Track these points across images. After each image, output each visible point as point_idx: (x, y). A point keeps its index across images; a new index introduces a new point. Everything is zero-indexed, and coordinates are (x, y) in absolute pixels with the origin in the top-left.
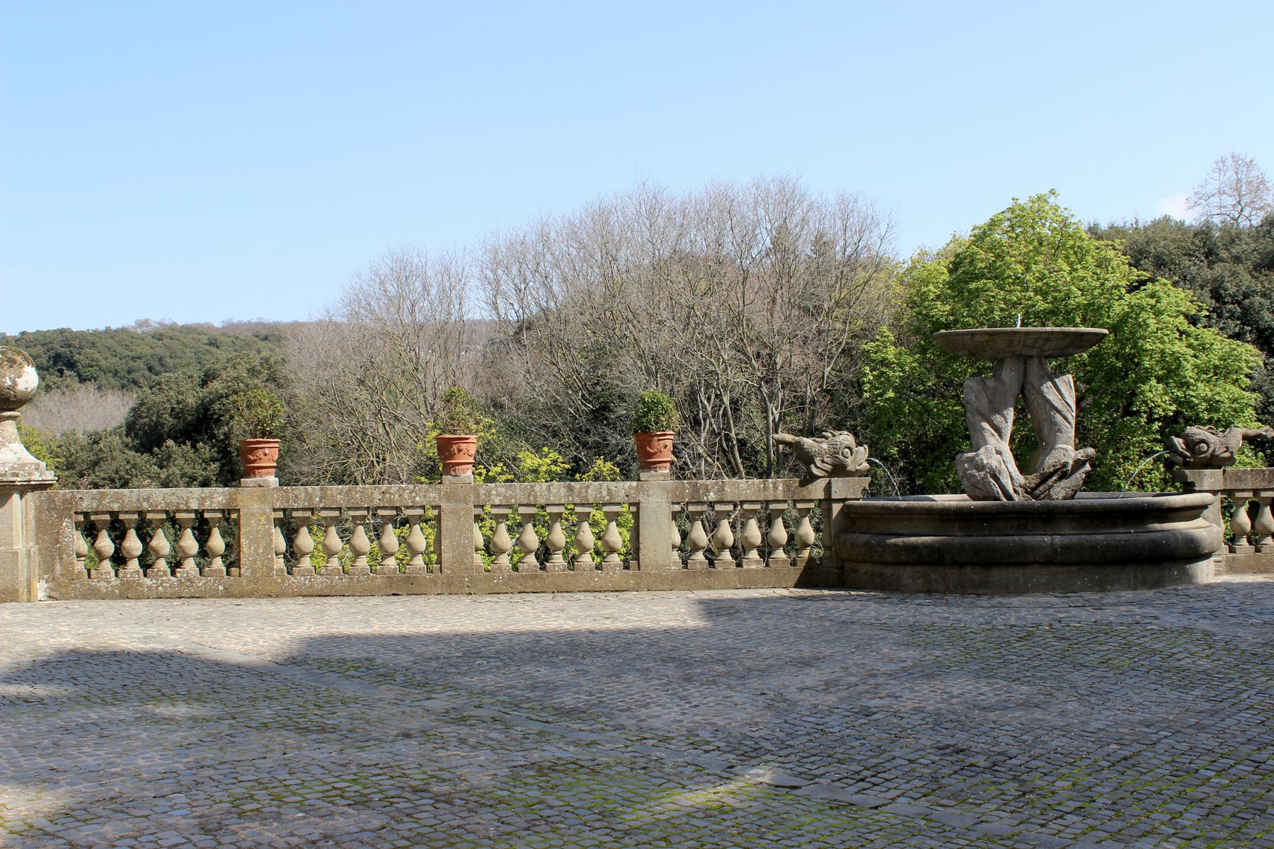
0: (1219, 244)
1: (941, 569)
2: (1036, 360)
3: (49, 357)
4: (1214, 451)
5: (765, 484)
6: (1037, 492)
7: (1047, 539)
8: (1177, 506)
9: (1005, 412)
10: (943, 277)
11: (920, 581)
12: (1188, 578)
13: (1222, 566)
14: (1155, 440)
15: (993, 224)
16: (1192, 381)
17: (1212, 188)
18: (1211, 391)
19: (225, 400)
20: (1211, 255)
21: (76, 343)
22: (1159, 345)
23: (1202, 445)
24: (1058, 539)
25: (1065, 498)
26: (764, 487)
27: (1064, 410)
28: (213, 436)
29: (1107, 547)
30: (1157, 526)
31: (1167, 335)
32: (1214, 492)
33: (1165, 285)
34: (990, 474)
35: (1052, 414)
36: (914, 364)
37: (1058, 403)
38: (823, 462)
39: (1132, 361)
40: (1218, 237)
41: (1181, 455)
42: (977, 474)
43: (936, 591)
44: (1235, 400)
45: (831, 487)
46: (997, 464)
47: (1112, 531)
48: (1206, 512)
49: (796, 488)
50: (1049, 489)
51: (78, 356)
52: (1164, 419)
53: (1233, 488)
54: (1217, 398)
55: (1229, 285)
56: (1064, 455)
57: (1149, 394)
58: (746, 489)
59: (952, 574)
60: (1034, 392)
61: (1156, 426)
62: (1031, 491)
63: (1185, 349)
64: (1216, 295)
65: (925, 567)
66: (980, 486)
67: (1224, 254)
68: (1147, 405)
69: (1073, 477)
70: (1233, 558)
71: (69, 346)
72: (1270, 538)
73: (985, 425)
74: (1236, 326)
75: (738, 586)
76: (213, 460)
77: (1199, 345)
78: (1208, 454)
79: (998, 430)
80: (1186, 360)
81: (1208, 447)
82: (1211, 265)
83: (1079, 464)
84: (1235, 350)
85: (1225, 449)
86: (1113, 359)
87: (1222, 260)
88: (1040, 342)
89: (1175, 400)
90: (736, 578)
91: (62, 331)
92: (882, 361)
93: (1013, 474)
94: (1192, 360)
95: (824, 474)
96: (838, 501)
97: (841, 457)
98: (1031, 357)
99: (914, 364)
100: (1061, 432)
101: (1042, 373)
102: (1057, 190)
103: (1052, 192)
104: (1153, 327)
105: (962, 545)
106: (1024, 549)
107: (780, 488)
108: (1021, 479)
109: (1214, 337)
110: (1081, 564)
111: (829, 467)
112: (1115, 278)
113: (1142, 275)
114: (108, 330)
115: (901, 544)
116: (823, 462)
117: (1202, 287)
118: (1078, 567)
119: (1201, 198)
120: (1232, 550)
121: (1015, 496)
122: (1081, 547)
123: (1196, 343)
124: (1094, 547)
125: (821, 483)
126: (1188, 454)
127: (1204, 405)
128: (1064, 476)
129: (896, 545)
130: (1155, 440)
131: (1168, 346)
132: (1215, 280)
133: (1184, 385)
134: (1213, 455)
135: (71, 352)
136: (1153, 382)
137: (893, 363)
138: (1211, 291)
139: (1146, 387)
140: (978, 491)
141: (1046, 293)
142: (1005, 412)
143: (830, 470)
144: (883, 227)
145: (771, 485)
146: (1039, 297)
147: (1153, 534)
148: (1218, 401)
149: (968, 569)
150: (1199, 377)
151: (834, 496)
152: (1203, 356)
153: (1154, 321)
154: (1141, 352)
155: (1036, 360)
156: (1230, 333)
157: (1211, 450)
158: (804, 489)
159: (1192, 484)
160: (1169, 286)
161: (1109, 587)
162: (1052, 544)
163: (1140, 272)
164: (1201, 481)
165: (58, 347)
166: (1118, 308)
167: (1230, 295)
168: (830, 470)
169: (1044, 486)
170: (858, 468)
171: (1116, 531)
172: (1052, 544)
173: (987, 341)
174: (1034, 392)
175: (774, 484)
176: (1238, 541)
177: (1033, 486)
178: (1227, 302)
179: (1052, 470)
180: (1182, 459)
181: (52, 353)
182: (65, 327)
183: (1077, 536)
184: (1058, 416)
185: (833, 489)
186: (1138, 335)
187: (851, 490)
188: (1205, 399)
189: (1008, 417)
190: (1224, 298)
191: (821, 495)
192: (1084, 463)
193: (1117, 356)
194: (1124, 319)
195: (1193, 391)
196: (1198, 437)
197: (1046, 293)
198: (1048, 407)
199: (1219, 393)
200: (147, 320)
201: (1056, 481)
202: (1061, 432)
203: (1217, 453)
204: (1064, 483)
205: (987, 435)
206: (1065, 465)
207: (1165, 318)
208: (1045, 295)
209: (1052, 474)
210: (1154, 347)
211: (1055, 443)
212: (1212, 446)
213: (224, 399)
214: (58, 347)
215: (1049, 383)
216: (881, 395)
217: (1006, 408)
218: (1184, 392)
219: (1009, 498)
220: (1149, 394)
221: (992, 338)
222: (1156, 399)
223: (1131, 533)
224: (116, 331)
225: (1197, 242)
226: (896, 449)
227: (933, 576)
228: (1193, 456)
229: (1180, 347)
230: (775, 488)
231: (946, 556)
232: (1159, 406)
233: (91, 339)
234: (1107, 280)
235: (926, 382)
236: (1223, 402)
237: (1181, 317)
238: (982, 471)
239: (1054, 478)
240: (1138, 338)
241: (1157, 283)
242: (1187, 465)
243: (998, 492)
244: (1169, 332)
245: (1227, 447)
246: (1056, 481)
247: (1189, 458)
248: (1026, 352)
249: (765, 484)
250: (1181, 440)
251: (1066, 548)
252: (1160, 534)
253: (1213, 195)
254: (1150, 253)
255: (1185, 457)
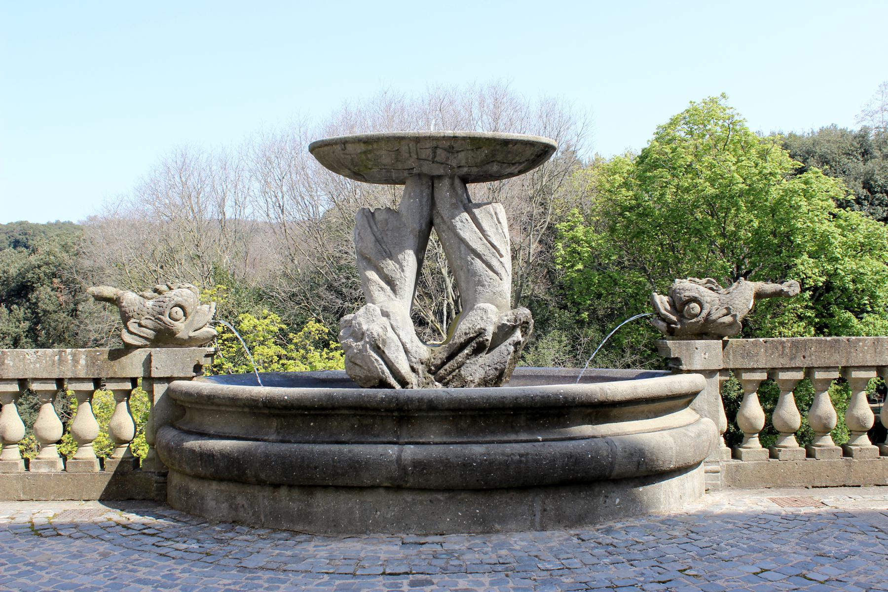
0: (874, 145)
1: (249, 490)
2: (446, 182)
3: (10, 242)
4: (709, 314)
5: (61, 356)
6: (442, 371)
7: (392, 451)
8: (619, 398)
9: (400, 257)
10: (628, 168)
11: (224, 506)
12: (636, 508)
13: (720, 480)
14: (807, 307)
15: (674, 122)
16: (839, 256)
17: (876, 106)
18: (857, 264)
19: (37, 270)
20: (866, 154)
21: (31, 232)
22: (809, 224)
23: (693, 305)
24: (410, 452)
25: (485, 382)
26: (59, 359)
27: (486, 253)
28: (29, 300)
29: (488, 465)
30: (587, 429)
31: (817, 216)
32: (709, 373)
33: (817, 173)
34: (371, 345)
35: (469, 259)
36: (600, 241)
37: (477, 244)
38: (140, 325)
39: (788, 237)
40: (873, 140)
41: (664, 319)
42: (354, 345)
43: (242, 523)
44: (877, 273)
45: (151, 362)
46: (380, 331)
47: (505, 438)
48: (697, 401)
49: (104, 361)
50: (459, 367)
51: (31, 242)
52: (815, 289)
53: (738, 366)
54: (861, 270)
55: (878, 177)
56: (482, 319)
57: (801, 267)
58: (35, 363)
59: (264, 498)
60: (445, 228)
61: (807, 294)
62: (435, 370)
63: (833, 228)
64: (867, 185)
65: (231, 485)
66: (358, 362)
67: (877, 153)
68: (800, 276)
69: (497, 350)
70: (737, 466)
71: (26, 234)
72: (792, 438)
73: (372, 275)
74: (884, 211)
75: (22, 497)
76: (26, 319)
77: (848, 226)
78: (700, 318)
79: (390, 282)
80: (834, 237)
81: (702, 308)
82: (865, 161)
83: (504, 332)
84: (878, 229)
85: (725, 311)
86: (771, 237)
87: (875, 157)
88: (441, 155)
89: (823, 273)
90: (19, 486)
91: (21, 223)
92: (572, 238)
93: (408, 346)
94: (840, 238)
95: (144, 342)
96: (161, 380)
97: (166, 319)
98: (440, 177)
99: (600, 241)
100: (483, 286)
101: (454, 201)
102: (728, 94)
103: (723, 96)
104: (804, 209)
105: (267, 456)
106: (356, 466)
107: (82, 362)
108: (422, 351)
109: (860, 218)
110: (450, 489)
111: (150, 334)
112: (772, 167)
113: (796, 164)
114: (57, 223)
115: (197, 449)
116: (140, 325)
117: (855, 180)
118: (447, 495)
119: (867, 115)
120: (735, 455)
121: (411, 377)
122: (445, 465)
123: (844, 224)
124: (466, 465)
125: (139, 356)
126: (674, 318)
127: (849, 278)
128: (480, 349)
129: (192, 451)
130: (807, 307)
131: (818, 225)
132: (868, 173)
133: (833, 260)
134: (707, 319)
135: (27, 239)
136: (805, 257)
137: (582, 240)
138: (864, 183)
139: (798, 261)
140: (358, 368)
141: (714, 180)
142: (400, 257)
143: (152, 337)
144: (580, 125)
145: (70, 357)
146: (707, 184)
147: (571, 444)
148: (861, 274)
149: (283, 492)
150: (847, 253)
151: (155, 374)
152: (851, 236)
153: (806, 204)
154: (793, 231)
155: (446, 182)
156: (880, 217)
157: (704, 313)
158: (116, 363)
159: (677, 360)
160: (820, 174)
161: (498, 527)
162: (399, 460)
163: (795, 162)
164: (691, 356)
165: (17, 235)
166: (775, 193)
167: (879, 186)
168: (152, 337)
169: (451, 362)
170: (192, 334)
171: (513, 437)
172: (399, 460)
173: (365, 152)
174: (445, 228)
175: (74, 355)
176: (746, 443)
177: (439, 362)
178: (877, 192)
179: (462, 340)
180: (665, 325)
181: (12, 239)
182: (23, 219)
183: (442, 447)
184: (478, 263)
185: (153, 364)
186: (792, 215)
187: (179, 366)
188: (852, 272)
189: (405, 264)
190: (874, 188)
191: (138, 372)
192: (513, 329)
193: (774, 234)
194: (779, 202)
195: (841, 264)
196: (687, 294)
197: (714, 180)
198: (463, 248)
199: (863, 267)
200: (95, 216)
201: (468, 356)
202: (483, 286)
203: (713, 317)
204: (484, 358)
205: (374, 289)
206: (481, 333)
207: (815, 201)
208: (712, 181)
209: (462, 346)
210: (805, 226)
211: (475, 301)
212: (707, 307)
213: (37, 269)
214: (17, 235)
215: (465, 215)
216: (572, 266)
217: (402, 250)
218: (834, 266)
219: (404, 383)
220: (801, 267)
221: (370, 147)
222: (807, 271)
223: (538, 441)
224: (64, 224)
225: (855, 143)
226: (587, 313)
227: (240, 500)
228: (680, 321)
229: (827, 226)
230: (76, 361)
231: (248, 471)
232: (810, 277)
233: (42, 229)
234: (765, 168)
235: (611, 256)
236: (866, 274)
237: (830, 200)
238: (362, 339)
239: (466, 351)
240: (793, 218)
241: (810, 172)
242: (672, 333)
243: (383, 372)
244: (819, 213)
245: (728, 309)
246: (468, 356)
247: (675, 323)
248: (426, 168)
249: (61, 356)
250: (666, 299)
251: (420, 466)
252: (583, 443)
253: (877, 112)
254: (816, 153)
255: (669, 322)
